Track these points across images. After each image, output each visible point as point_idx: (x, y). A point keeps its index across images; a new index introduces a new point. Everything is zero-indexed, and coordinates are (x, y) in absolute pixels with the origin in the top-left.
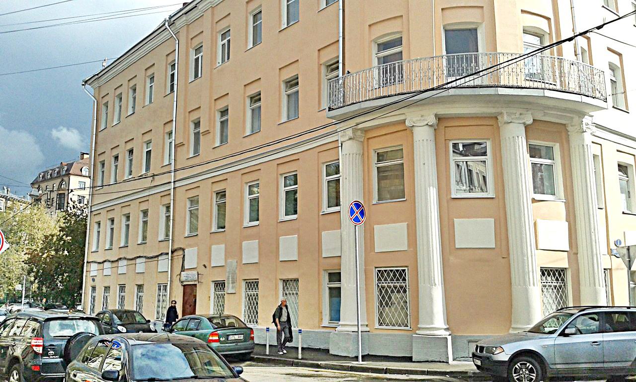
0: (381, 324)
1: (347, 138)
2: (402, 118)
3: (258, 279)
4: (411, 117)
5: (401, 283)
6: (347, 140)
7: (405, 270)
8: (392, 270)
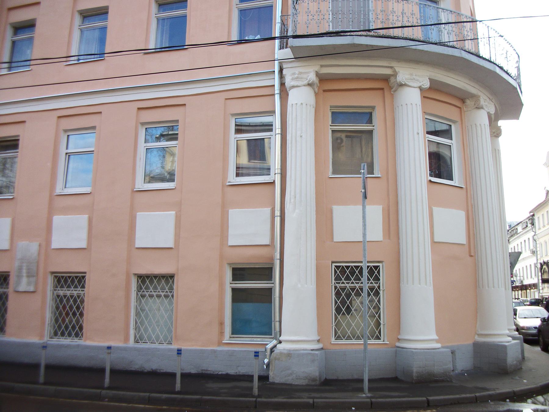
0: (338, 338)
1: (306, 82)
2: (388, 72)
3: (85, 273)
4: (403, 73)
5: (151, 292)
6: (304, 86)
7: (378, 266)
8: (78, 276)
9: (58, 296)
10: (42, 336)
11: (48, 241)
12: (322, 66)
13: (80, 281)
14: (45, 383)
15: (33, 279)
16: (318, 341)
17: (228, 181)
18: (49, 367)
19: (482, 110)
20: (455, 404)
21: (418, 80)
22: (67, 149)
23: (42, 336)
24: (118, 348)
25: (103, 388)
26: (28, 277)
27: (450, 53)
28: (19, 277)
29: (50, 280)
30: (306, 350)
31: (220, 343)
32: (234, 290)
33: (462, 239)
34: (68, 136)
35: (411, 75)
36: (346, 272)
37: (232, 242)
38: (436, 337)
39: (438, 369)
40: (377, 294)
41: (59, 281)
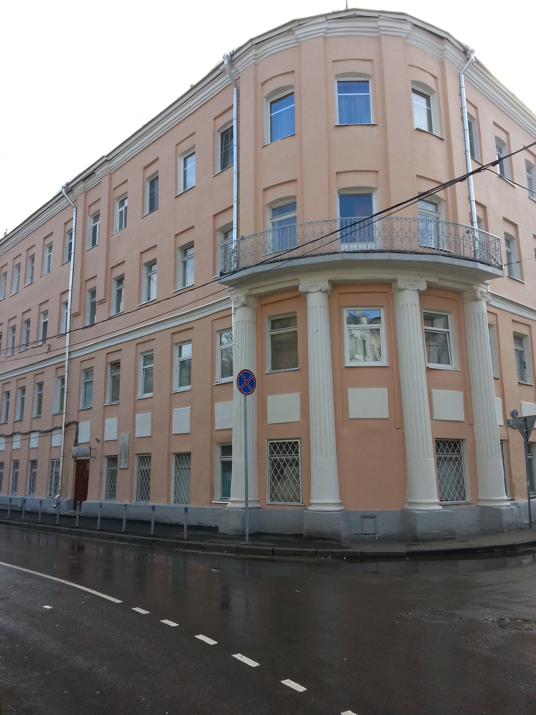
2: (294, 284)
9: (275, 461)
10: (131, 500)
11: (134, 433)
12: (251, 289)
14: (100, 530)
16: (341, 504)
17: (216, 381)
18: (103, 519)
19: (406, 291)
20: (296, 555)
21: (317, 286)
24: (164, 507)
25: (96, 530)
26: (124, 458)
27: (331, 260)
29: (136, 459)
30: (238, 508)
31: (211, 504)
33: (384, 413)
34: (221, 334)
36: (276, 447)
37: (217, 427)
40: (297, 465)
41: (275, 448)
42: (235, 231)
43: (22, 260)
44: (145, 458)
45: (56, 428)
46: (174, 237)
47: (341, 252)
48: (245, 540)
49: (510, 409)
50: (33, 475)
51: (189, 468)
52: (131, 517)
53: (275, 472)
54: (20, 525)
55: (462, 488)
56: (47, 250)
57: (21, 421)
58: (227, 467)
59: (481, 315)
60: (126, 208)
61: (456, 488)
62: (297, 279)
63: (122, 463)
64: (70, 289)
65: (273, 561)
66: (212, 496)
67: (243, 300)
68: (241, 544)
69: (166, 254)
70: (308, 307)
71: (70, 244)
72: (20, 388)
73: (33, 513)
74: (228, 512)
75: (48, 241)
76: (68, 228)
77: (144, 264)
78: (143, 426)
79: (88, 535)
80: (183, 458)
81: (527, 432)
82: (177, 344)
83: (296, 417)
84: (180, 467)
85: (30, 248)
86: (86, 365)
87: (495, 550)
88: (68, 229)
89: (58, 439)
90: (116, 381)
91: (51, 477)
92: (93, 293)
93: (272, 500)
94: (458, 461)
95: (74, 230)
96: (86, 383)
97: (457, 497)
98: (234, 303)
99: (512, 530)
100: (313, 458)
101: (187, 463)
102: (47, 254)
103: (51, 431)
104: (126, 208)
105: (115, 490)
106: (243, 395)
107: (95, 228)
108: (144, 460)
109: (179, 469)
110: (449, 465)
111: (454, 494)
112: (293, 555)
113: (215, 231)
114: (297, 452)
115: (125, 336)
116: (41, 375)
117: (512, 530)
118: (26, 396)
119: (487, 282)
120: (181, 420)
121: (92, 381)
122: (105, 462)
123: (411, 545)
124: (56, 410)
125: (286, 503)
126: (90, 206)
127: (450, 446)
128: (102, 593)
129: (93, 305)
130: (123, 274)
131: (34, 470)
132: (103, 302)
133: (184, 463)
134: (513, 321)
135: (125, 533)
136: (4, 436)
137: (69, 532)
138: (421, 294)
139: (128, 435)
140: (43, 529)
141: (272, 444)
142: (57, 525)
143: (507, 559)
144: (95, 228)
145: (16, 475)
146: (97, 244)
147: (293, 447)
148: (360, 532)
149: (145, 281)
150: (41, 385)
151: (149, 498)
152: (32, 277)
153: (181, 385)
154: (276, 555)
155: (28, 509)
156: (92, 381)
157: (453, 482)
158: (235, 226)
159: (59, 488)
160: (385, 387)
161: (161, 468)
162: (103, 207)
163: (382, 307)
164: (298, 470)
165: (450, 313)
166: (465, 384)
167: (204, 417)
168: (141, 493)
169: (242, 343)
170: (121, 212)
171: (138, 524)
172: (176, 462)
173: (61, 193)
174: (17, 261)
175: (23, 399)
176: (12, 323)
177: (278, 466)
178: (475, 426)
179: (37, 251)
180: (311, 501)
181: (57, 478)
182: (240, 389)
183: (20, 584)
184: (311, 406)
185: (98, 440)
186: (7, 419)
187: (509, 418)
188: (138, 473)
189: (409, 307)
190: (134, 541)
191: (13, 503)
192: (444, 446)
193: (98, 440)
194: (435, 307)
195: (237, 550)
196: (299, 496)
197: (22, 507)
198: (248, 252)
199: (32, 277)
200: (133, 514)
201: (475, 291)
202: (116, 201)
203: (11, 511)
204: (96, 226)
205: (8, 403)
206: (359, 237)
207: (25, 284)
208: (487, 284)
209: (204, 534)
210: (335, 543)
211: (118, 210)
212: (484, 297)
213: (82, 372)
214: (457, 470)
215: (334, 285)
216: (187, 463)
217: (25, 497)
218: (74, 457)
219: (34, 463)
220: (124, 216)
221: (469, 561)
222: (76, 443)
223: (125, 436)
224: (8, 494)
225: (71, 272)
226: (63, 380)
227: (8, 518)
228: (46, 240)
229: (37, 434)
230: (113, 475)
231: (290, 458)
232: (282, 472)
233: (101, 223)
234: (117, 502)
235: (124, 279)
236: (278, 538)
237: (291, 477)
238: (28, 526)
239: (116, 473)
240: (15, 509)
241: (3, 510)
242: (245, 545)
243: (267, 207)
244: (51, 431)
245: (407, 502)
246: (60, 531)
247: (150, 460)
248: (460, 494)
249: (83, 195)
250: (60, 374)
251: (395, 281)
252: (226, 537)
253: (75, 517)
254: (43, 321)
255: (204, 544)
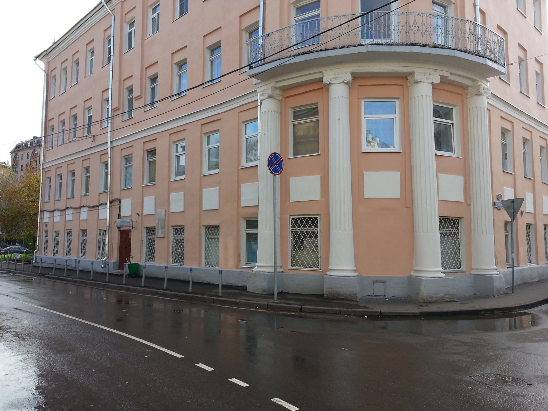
2: (318, 76)
9: (296, 233)
10: (168, 263)
11: (169, 208)
12: (277, 82)
13: (313, 222)
14: (144, 287)
15: (163, 230)
16: (355, 271)
17: (242, 165)
18: (169, 280)
20: (321, 313)
21: (340, 78)
22: (208, 144)
23: (168, 263)
24: (197, 269)
25: (141, 287)
28: (158, 229)
29: (171, 230)
31: (238, 267)
32: (247, 234)
35: (335, 74)
37: (243, 205)
38: (441, 269)
39: (344, 291)
40: (316, 237)
41: (296, 222)
42: (261, 29)
43: (69, 64)
44: (179, 230)
45: (102, 204)
46: (202, 37)
47: (366, 45)
48: (273, 298)
49: (496, 193)
50: (84, 242)
51: (218, 239)
52: (171, 277)
53: (296, 243)
54: (75, 282)
55: (458, 258)
56: (89, 54)
57: (72, 198)
58: (252, 238)
59: (482, 108)
60: (158, 14)
61: (454, 259)
62: (321, 72)
63: (159, 233)
64: (110, 87)
65: (301, 317)
66: (239, 261)
67: (269, 92)
68: (271, 302)
69: (195, 55)
70: (330, 98)
71: (110, 49)
72: (71, 171)
73: (85, 272)
74: (256, 274)
75: (90, 47)
76: (107, 34)
77: (175, 64)
78: (177, 202)
79: (135, 291)
80: (212, 230)
81: (514, 212)
82: (206, 134)
83: (315, 195)
84: (210, 237)
85: (75, 54)
86: (125, 152)
87: (496, 312)
88: (107, 36)
89: (104, 213)
90: (152, 164)
91: (99, 243)
92: (130, 91)
93: (293, 266)
94: (456, 236)
95: (112, 35)
96: (126, 168)
97: (454, 267)
98: (261, 95)
99: (500, 294)
100: (333, 231)
101: (216, 234)
102: (89, 59)
103: (98, 206)
104: (158, 14)
105: (154, 255)
106: (272, 175)
107: (130, 34)
108: (178, 231)
109: (208, 239)
110: (448, 239)
111: (452, 263)
112: (319, 312)
113: (241, 30)
114: (316, 226)
115: (159, 127)
116: (88, 161)
117: (500, 294)
118: (75, 178)
119: (489, 79)
120: (211, 198)
121: (132, 166)
122: (145, 232)
123: (420, 306)
124: (102, 189)
125: (305, 269)
126: (126, 14)
127: (450, 223)
128: (162, 347)
129: (130, 101)
130: (157, 73)
131: (85, 238)
132: (139, 98)
133: (213, 234)
134: (502, 117)
135: (166, 290)
136: (59, 210)
137: (117, 288)
138: (435, 87)
139: (164, 210)
140: (95, 285)
141: (293, 219)
142: (107, 282)
143: (496, 320)
144: (130, 34)
145: (70, 241)
146: (133, 47)
147: (313, 222)
148: (372, 294)
149: (176, 79)
150: (87, 169)
151: (183, 262)
152: (77, 79)
153: (210, 168)
154: (304, 312)
155: (80, 269)
156: (132, 166)
157: (451, 253)
158: (261, 24)
159: (106, 252)
160: (397, 171)
161: (193, 237)
162: (137, 14)
163: (398, 98)
164: (318, 242)
165: (455, 106)
166: (465, 169)
167: (232, 196)
168: (176, 258)
169: (266, 130)
170: (154, 19)
171: (177, 283)
172: (206, 233)
173: (101, 3)
174: (64, 66)
175: (73, 181)
176: (62, 118)
177: (299, 237)
178: (472, 206)
179: (81, 56)
180: (330, 267)
181: (104, 244)
182: (270, 170)
183: (83, 336)
184: (334, 186)
185: (138, 214)
186: (60, 196)
187: (496, 200)
188: (173, 242)
189: (423, 96)
190: (175, 296)
191: (68, 264)
192: (445, 222)
193: (138, 214)
194: (446, 100)
195: (268, 307)
196: (318, 264)
197: (75, 267)
198: (276, 45)
199: (77, 79)
200: (172, 274)
201: (479, 87)
202: (149, 8)
203: (67, 270)
204: (131, 32)
205: (61, 183)
206: (383, 30)
207: (71, 84)
208: (488, 82)
209: (234, 294)
210: (353, 303)
211: (151, 17)
212: (486, 92)
213: (123, 158)
214: (455, 243)
215: (356, 77)
216: (216, 234)
217: (79, 259)
218: (118, 228)
219: (84, 232)
220: (156, 22)
221: (465, 321)
222: (119, 216)
223: (162, 212)
224: (64, 256)
225: (111, 72)
226: (107, 165)
227: (65, 275)
228: (88, 46)
229: (86, 209)
230: (151, 244)
231: (310, 231)
232: (302, 243)
233: (137, 29)
234: (187, 266)
235: (157, 77)
236: (300, 297)
237: (311, 247)
238: (83, 283)
239: (154, 241)
240: (70, 268)
241: (49, 268)
242: (274, 303)
243: (292, 6)
244: (98, 206)
245: (414, 270)
246: (109, 287)
247: (183, 231)
248: (456, 264)
249: (120, 3)
250: (104, 159)
251: (412, 74)
252: (253, 295)
253: (122, 275)
254: (87, 115)
255: (238, 301)
